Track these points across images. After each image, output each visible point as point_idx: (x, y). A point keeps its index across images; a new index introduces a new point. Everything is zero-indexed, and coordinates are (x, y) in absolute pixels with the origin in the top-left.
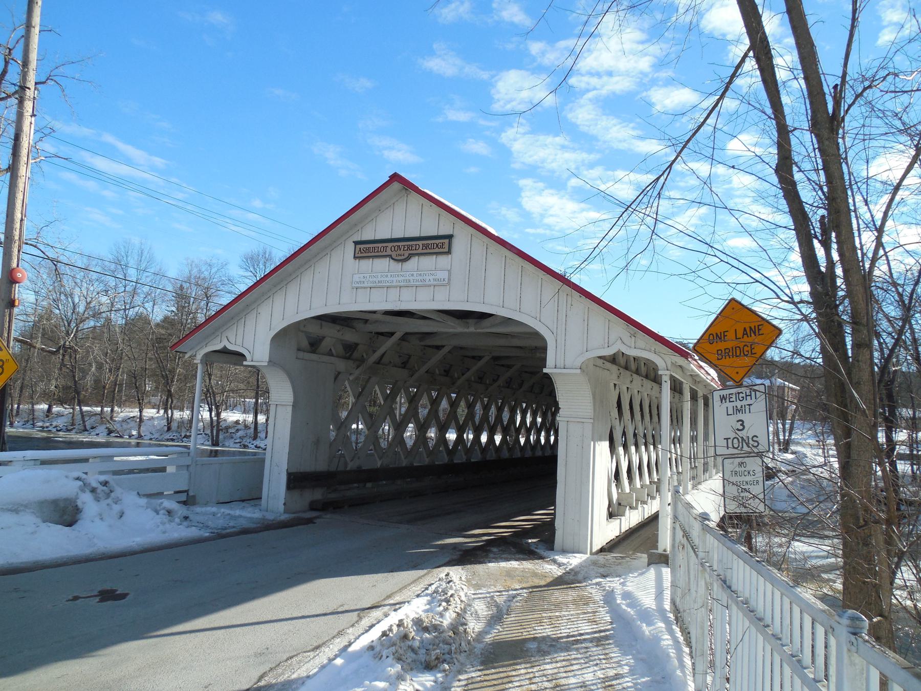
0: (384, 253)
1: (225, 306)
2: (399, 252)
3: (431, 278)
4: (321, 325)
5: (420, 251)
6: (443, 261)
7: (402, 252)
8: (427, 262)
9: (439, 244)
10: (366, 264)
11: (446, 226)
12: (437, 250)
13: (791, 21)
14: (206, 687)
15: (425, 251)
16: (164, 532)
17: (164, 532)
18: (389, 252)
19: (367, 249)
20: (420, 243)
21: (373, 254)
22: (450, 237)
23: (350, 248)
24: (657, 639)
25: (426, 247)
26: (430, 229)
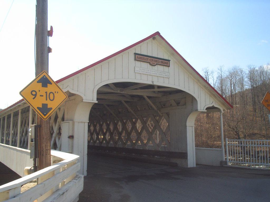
0: (147, 61)
1: (208, 83)
2: (153, 62)
3: (164, 74)
4: (153, 82)
5: (160, 63)
6: (166, 69)
7: (154, 62)
8: (160, 68)
9: (165, 63)
10: (138, 63)
11: (175, 62)
12: (166, 65)
13: (202, 77)
14: (185, 88)
15: (162, 64)
16: (33, 146)
17: (33, 146)
18: (149, 61)
19: (139, 57)
20: (160, 60)
21: (143, 60)
22: (169, 61)
23: (132, 57)
24: (143, 139)
25: (162, 62)
26: (166, 57)
